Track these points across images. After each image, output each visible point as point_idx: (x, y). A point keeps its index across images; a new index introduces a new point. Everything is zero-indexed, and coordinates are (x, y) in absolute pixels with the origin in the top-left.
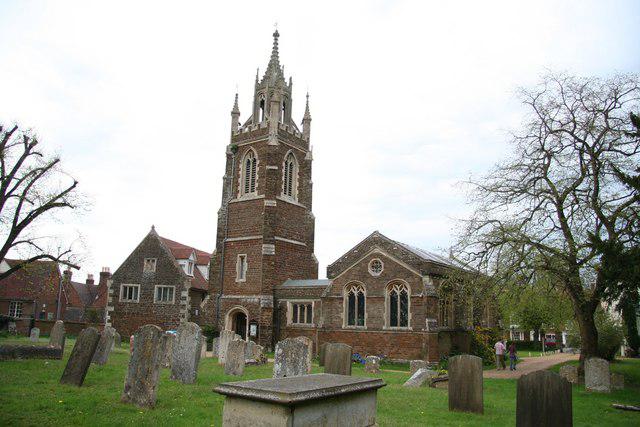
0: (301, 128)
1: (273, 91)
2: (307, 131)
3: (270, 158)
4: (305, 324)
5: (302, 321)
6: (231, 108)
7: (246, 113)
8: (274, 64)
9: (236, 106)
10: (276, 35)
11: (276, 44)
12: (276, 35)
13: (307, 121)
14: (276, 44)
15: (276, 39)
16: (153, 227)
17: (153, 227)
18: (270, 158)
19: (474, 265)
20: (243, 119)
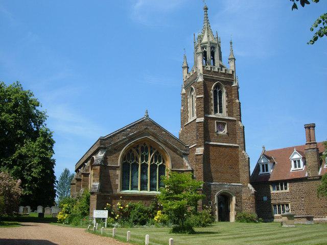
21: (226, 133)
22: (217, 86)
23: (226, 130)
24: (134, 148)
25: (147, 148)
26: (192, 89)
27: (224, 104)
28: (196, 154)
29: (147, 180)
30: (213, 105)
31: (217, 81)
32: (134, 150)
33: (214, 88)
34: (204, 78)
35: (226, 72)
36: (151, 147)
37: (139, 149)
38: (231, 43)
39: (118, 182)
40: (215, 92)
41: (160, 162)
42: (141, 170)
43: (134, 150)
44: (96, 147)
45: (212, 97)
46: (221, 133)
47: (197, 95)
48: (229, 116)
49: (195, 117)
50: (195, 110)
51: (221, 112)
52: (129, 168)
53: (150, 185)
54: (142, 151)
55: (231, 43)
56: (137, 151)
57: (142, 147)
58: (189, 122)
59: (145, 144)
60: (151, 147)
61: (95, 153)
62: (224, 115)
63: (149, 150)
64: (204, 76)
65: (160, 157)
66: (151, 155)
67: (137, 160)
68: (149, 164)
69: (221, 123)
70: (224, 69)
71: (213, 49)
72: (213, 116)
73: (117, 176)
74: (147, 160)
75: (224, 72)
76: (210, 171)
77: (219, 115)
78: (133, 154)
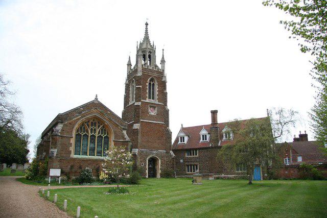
0: (160, 66)
1: (146, 52)
2: (163, 67)
3: (146, 80)
4: (195, 156)
5: (193, 155)
6: (127, 62)
7: (133, 63)
8: (147, 38)
9: (163, 57)
10: (147, 24)
11: (146, 28)
12: (147, 24)
13: (163, 61)
14: (146, 28)
15: (147, 26)
16: (96, 96)
17: (96, 96)
18: (146, 80)
19: (273, 122)
20: (132, 67)
22: (152, 80)
27: (157, 93)
29: (95, 148)
37: (90, 124)
39: (72, 149)
40: (150, 84)
45: (148, 87)
46: (152, 114)
56: (88, 125)
57: (92, 123)
65: (105, 130)
67: (87, 132)
68: (97, 136)
69: (153, 106)
72: (147, 100)
74: (95, 133)
77: (152, 101)
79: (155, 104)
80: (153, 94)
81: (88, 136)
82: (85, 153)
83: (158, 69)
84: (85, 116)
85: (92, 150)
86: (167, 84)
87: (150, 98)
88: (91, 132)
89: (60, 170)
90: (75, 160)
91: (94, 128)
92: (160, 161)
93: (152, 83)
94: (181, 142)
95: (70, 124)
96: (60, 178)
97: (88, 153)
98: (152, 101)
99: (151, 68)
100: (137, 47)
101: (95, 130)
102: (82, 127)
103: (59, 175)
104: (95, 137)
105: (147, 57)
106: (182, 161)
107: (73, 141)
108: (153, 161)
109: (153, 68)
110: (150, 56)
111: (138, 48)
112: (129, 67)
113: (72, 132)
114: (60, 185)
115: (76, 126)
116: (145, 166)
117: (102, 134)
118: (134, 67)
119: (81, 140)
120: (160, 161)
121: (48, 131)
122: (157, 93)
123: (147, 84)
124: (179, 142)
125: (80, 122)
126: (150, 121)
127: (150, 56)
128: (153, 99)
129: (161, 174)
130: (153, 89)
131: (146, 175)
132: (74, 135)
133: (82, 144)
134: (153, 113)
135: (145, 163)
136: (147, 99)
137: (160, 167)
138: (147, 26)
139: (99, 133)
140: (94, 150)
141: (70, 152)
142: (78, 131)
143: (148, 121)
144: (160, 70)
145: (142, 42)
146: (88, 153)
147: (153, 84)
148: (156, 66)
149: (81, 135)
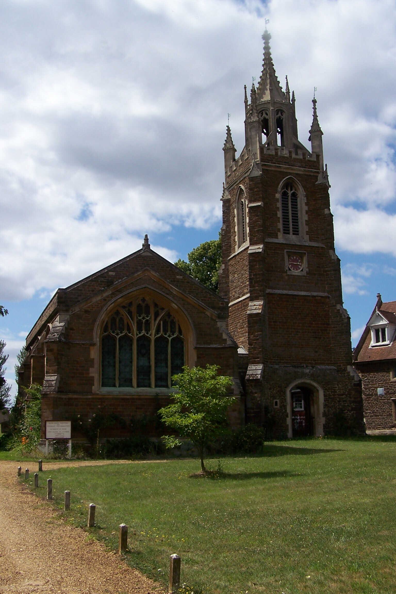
7: (240, 144)
15: (315, 105)
21: (304, 273)
22: (289, 185)
23: (304, 266)
24: (124, 307)
25: (147, 307)
26: (241, 190)
27: (303, 217)
28: (248, 312)
29: (150, 367)
30: (281, 220)
31: (287, 174)
32: (124, 312)
33: (283, 188)
34: (263, 170)
35: (304, 158)
36: (156, 305)
37: (134, 309)
38: (314, 102)
39: (95, 372)
40: (285, 194)
41: (173, 333)
42: (138, 350)
43: (124, 312)
44: (52, 309)
45: (279, 205)
46: (296, 272)
47: (250, 201)
48: (311, 240)
49: (247, 244)
50: (186, 313)
51: (296, 232)
52: (115, 345)
53: (156, 376)
54: (139, 313)
55: (314, 102)
56: (130, 313)
57: (139, 306)
58: (236, 253)
59: (144, 300)
60: (156, 305)
61: (51, 319)
62: (302, 238)
63: (152, 310)
64: (263, 165)
65: (173, 323)
66: (155, 319)
67: (129, 329)
68: (153, 338)
69: (297, 252)
70: (300, 152)
71: (280, 114)
72: (281, 239)
73: (278, 208)
74: (148, 330)
75: (301, 157)
76: (312, 453)
77: (293, 238)
78: (121, 320)
79: (301, 247)
80: (295, 220)
81: (131, 340)
82: (127, 382)
83: (304, 155)
84: (120, 291)
85: (143, 374)
86: (330, 191)
87: (286, 232)
88: (139, 329)
89: (69, 423)
90: (102, 400)
91: (143, 318)
92: (321, 394)
93: (290, 193)
94: (378, 341)
95: (86, 311)
96: (70, 441)
97: (117, 384)
98: (293, 238)
99: (285, 153)
100: (246, 102)
101: (148, 323)
102: (115, 321)
103: (68, 435)
104: (149, 340)
105: (272, 123)
106: (380, 391)
107: (95, 354)
108: (306, 394)
109: (290, 152)
110: (279, 123)
111: (249, 102)
112: (230, 155)
113: (92, 330)
114: (71, 460)
115: (103, 317)
116: (285, 407)
117: (165, 331)
118: (242, 156)
119: (115, 349)
120: (321, 394)
121: (39, 333)
122: (303, 217)
123: (278, 196)
124: (373, 343)
125: (110, 306)
126: (291, 292)
127: (279, 123)
128: (296, 232)
129: (325, 427)
130: (295, 205)
131: (287, 430)
132: (97, 340)
133: (117, 360)
134: (300, 269)
135: (284, 400)
136: (280, 235)
137: (322, 409)
138: (315, 105)
139: (158, 331)
140: (150, 372)
141: (90, 381)
142: (106, 329)
143: (285, 292)
144: (311, 155)
145: (257, 86)
146: (117, 384)
147: (294, 195)
148: (299, 147)
149: (114, 339)
